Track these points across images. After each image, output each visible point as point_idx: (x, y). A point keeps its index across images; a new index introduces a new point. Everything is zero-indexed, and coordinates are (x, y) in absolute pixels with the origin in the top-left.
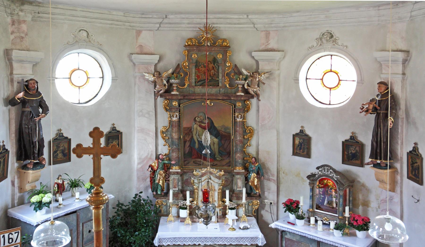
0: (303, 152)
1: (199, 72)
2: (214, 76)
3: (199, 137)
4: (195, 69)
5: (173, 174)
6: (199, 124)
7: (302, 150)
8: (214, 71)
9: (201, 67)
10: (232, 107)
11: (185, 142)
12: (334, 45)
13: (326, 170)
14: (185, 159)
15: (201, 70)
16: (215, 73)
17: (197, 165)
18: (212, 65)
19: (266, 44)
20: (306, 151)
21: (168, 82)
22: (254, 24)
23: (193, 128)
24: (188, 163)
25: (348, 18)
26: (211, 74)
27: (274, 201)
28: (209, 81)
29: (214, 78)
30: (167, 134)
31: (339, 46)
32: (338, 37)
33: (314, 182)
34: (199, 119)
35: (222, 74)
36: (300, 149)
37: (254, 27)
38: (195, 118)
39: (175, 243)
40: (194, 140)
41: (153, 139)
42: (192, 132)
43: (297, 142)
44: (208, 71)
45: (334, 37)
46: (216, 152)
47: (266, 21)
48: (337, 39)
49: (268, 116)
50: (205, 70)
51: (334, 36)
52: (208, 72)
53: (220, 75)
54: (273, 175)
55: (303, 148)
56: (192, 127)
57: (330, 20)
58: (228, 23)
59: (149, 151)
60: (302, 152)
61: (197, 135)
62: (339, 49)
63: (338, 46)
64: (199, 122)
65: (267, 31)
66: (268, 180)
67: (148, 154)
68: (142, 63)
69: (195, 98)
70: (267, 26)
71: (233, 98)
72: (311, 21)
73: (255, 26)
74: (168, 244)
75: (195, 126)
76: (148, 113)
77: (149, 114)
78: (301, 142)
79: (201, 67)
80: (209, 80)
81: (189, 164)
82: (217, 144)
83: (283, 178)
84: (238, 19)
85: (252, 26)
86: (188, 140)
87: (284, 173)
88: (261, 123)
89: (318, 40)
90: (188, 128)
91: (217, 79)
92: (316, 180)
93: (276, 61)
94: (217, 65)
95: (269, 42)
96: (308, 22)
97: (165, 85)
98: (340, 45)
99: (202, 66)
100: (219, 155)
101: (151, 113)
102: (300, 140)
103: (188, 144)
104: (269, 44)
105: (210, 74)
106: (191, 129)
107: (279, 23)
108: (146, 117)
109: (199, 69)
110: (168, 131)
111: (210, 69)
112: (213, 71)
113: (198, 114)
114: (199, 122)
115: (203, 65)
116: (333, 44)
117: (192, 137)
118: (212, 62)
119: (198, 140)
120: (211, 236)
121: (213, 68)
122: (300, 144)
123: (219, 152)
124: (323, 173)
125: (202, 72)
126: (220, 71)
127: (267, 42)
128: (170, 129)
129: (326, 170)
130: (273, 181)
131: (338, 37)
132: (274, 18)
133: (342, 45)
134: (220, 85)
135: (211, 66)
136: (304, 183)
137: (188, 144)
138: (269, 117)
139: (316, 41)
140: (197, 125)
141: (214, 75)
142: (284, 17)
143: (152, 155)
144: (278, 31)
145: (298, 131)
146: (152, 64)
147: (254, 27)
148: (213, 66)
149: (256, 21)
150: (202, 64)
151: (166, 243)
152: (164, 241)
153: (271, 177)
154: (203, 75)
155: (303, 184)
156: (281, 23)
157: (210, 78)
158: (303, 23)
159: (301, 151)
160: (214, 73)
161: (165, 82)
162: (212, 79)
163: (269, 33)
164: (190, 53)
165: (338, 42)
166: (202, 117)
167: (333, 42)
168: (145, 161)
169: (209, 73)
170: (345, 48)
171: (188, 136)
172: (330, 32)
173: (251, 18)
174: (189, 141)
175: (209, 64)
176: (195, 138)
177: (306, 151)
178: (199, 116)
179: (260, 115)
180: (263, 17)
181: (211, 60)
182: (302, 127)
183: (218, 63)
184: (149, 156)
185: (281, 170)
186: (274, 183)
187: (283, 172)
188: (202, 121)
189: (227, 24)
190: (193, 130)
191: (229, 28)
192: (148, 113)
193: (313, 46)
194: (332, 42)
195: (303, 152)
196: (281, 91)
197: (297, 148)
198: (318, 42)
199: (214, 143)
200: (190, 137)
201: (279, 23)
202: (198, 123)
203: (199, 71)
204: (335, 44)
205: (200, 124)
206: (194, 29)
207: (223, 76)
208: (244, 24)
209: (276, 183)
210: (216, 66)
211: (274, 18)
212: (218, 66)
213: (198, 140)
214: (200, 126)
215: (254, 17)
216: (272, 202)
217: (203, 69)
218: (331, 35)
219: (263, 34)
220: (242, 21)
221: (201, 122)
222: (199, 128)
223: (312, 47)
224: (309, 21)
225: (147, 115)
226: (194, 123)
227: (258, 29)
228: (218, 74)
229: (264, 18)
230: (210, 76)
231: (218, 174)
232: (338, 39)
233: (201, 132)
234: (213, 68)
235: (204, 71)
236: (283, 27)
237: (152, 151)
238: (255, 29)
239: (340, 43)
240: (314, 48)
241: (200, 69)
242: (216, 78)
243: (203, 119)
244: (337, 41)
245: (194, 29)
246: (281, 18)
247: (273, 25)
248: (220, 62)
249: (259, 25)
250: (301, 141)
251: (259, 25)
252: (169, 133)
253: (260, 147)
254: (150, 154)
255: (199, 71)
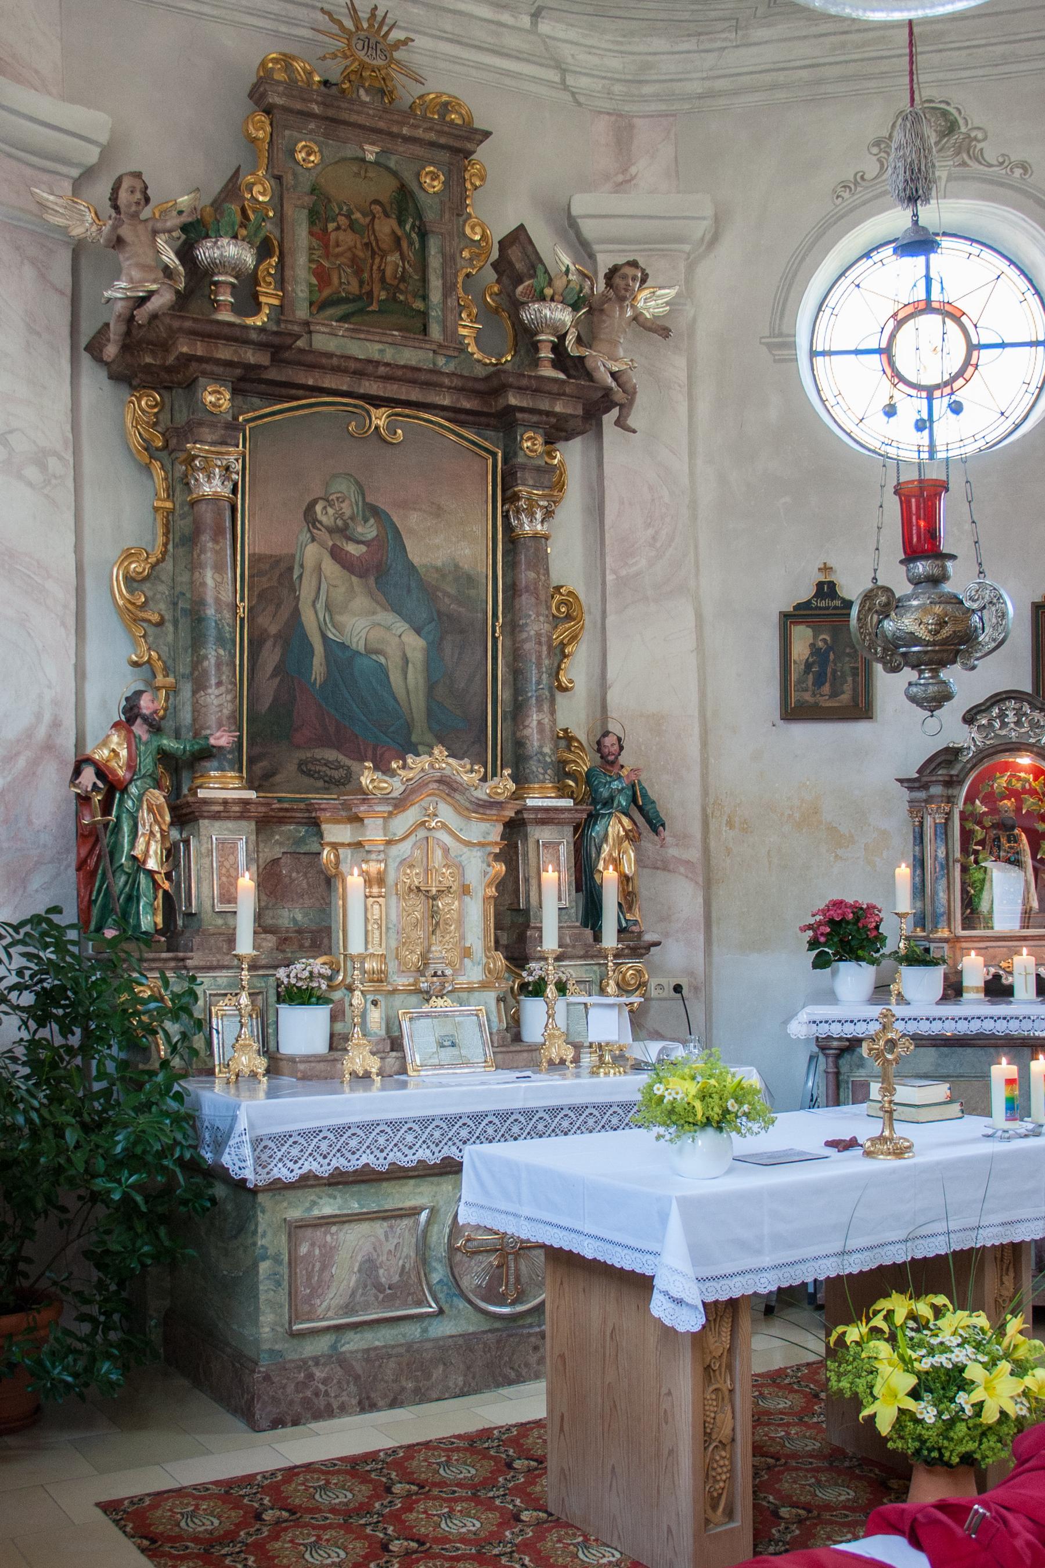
0: (834, 694)
1: (327, 255)
2: (402, 286)
3: (331, 618)
4: (311, 233)
5: (216, 817)
6: (330, 543)
7: (827, 685)
8: (403, 258)
9: (335, 224)
10: (495, 466)
11: (256, 644)
12: (964, 164)
13: (1011, 718)
14: (257, 750)
15: (338, 245)
16: (404, 268)
17: (320, 784)
18: (393, 223)
19: (620, 178)
20: (848, 687)
21: (185, 253)
22: (560, 67)
23: (302, 566)
24: (273, 774)
25: (1026, 36)
26: (389, 273)
27: (691, 974)
28: (380, 312)
29: (402, 298)
30: (149, 594)
31: (990, 166)
32: (979, 128)
33: (950, 792)
34: (330, 511)
35: (444, 276)
36: (819, 682)
37: (563, 81)
38: (313, 503)
39: (339, 1162)
40: (304, 637)
41: (63, 624)
42: (293, 589)
43: (800, 650)
44: (374, 253)
45: (963, 129)
46: (414, 710)
47: (615, 63)
48: (975, 139)
49: (650, 531)
50: (359, 246)
51: (961, 122)
52: (373, 258)
53: (435, 284)
54: (683, 839)
55: (834, 672)
56: (293, 556)
57: (940, 51)
58: (450, 36)
59: (40, 696)
60: (831, 697)
61: (318, 606)
62: (991, 182)
63: (986, 169)
64: (331, 531)
65: (620, 115)
66: (658, 868)
67: (39, 716)
68: (12, 146)
69: (320, 384)
70: (618, 88)
71: (515, 397)
72: (846, 62)
73: (568, 83)
74: (304, 1170)
75: (312, 552)
76: (40, 459)
77: (43, 467)
78: (820, 644)
79: (338, 228)
80: (380, 302)
81: (278, 778)
82: (420, 666)
83: (729, 852)
84: (493, 27)
85: (554, 76)
86: (273, 630)
87: (730, 824)
88: (614, 572)
89: (883, 146)
90: (276, 561)
91: (419, 305)
92: (961, 783)
93: (687, 248)
94: (413, 227)
95: (633, 170)
96: (831, 64)
97: (168, 272)
98: (995, 163)
99: (343, 221)
100: (430, 729)
101: (52, 463)
102: (815, 637)
103: (271, 657)
104: (630, 181)
105: (383, 272)
106: (291, 569)
107: (680, 80)
108: (30, 484)
109: (325, 229)
110: (157, 578)
111: (384, 246)
112: (394, 258)
113: (327, 485)
114: (331, 531)
115: (348, 216)
116: (958, 160)
117: (296, 613)
118: (388, 209)
119: (324, 637)
120: (531, 1104)
121: (397, 240)
122: (819, 655)
123: (430, 713)
124: (997, 736)
125: (341, 254)
126: (435, 262)
127: (625, 171)
128: (168, 565)
129: (1011, 718)
130: (682, 870)
131: (979, 128)
132: (655, 54)
133: (1002, 163)
134: (435, 332)
135: (387, 230)
136: (840, 852)
137: (271, 657)
138: (654, 538)
139: (875, 150)
140: (322, 545)
141: (403, 279)
142: (701, 47)
143: (56, 724)
144: (674, 115)
145: (806, 592)
146: (64, 169)
147: (563, 81)
148: (393, 232)
149: (573, 55)
150: (341, 209)
151: (290, 1164)
152: (279, 1154)
153: (673, 852)
154: (349, 270)
155: (837, 856)
156: (691, 79)
157: (383, 295)
158: (804, 74)
159: (826, 689)
160: (400, 269)
161: (169, 257)
162: (395, 299)
163: (631, 127)
164: (284, 137)
165: (982, 150)
166: (347, 502)
167: (958, 154)
168: (21, 762)
169: (375, 267)
170: (1018, 172)
171: (271, 608)
172: (943, 106)
173: (549, 37)
174: (278, 636)
175: (374, 217)
176: (309, 619)
177: (848, 687)
178: (333, 497)
179: (606, 527)
180: (604, 45)
181: (384, 198)
182: (826, 569)
183: (419, 216)
184: (41, 732)
185: (717, 813)
186: (692, 880)
187: (725, 818)
188: (346, 526)
189: (441, 38)
190: (301, 577)
191: (455, 60)
192: (40, 459)
193: (862, 177)
194: (950, 153)
195: (834, 694)
196: (704, 407)
197: (799, 682)
198: (883, 154)
199: (406, 661)
200: (285, 613)
201: (680, 80)
202: (323, 535)
203: (326, 246)
204: (969, 161)
205: (334, 545)
206: (283, 29)
207: (448, 289)
208: (518, 58)
209: (700, 880)
210: (408, 236)
211: (655, 54)
212: (423, 235)
213: (324, 637)
214: (336, 554)
215: (561, 35)
216: (684, 982)
217: (348, 239)
218: (946, 120)
219: (601, 127)
220: (512, 41)
221: (342, 531)
222: (330, 567)
223: (856, 183)
224: (837, 63)
225: (32, 472)
226: (305, 536)
227: (582, 99)
228: (424, 280)
229: (605, 50)
230: (383, 280)
231: (483, 793)
232: (980, 136)
233: (342, 589)
234: (397, 240)
235: (350, 249)
236: (700, 98)
237: (55, 703)
238: (567, 97)
239: (991, 156)
240: (863, 183)
241: (333, 236)
242: (410, 300)
243: (352, 518)
244: (979, 146)
245: (283, 29)
246: (689, 52)
247: (647, 89)
248: (430, 216)
249: (584, 82)
250: (824, 640)
251: (584, 82)
252: (162, 588)
253: (613, 697)
254: (47, 717)
255: (326, 246)
